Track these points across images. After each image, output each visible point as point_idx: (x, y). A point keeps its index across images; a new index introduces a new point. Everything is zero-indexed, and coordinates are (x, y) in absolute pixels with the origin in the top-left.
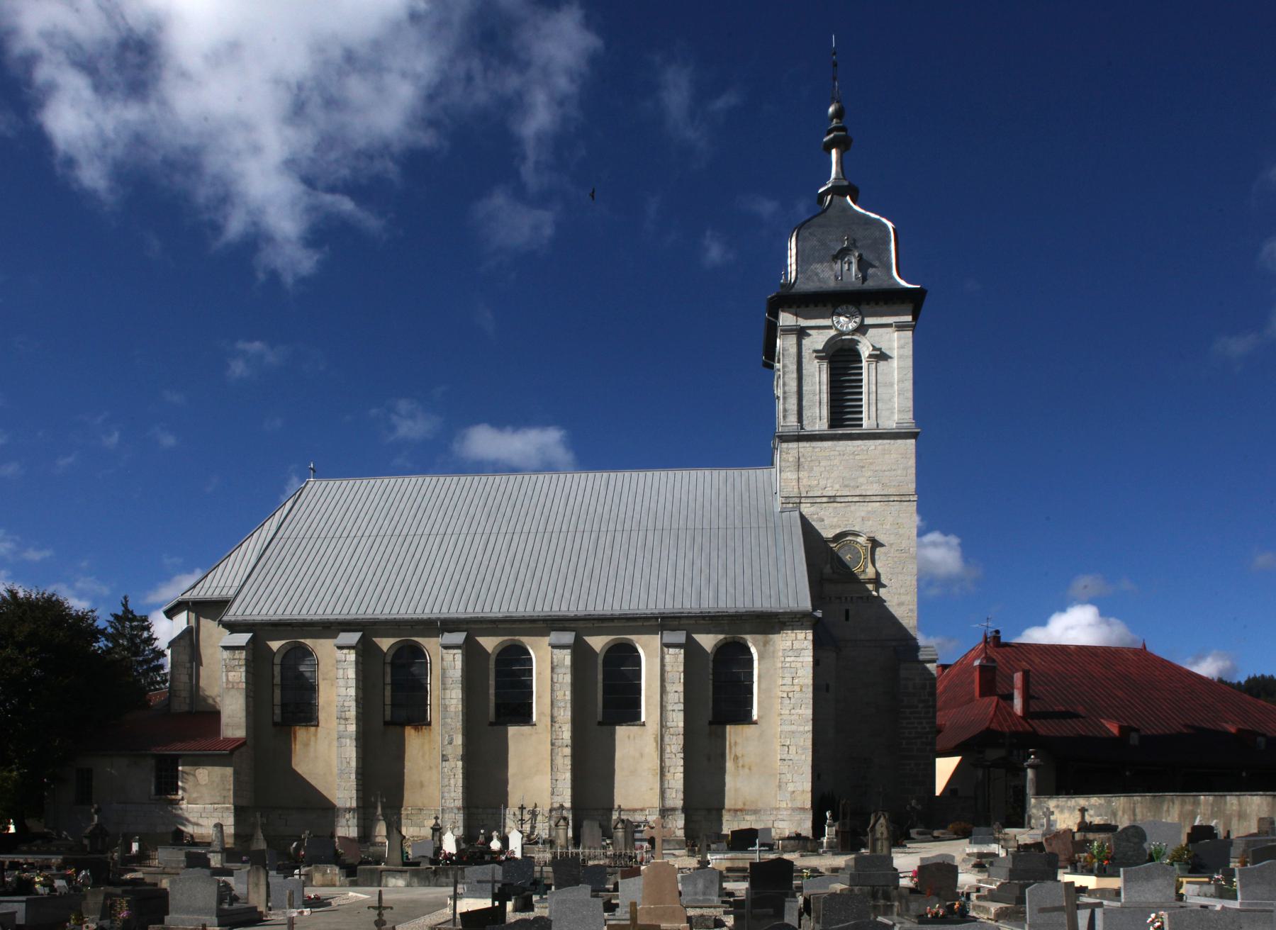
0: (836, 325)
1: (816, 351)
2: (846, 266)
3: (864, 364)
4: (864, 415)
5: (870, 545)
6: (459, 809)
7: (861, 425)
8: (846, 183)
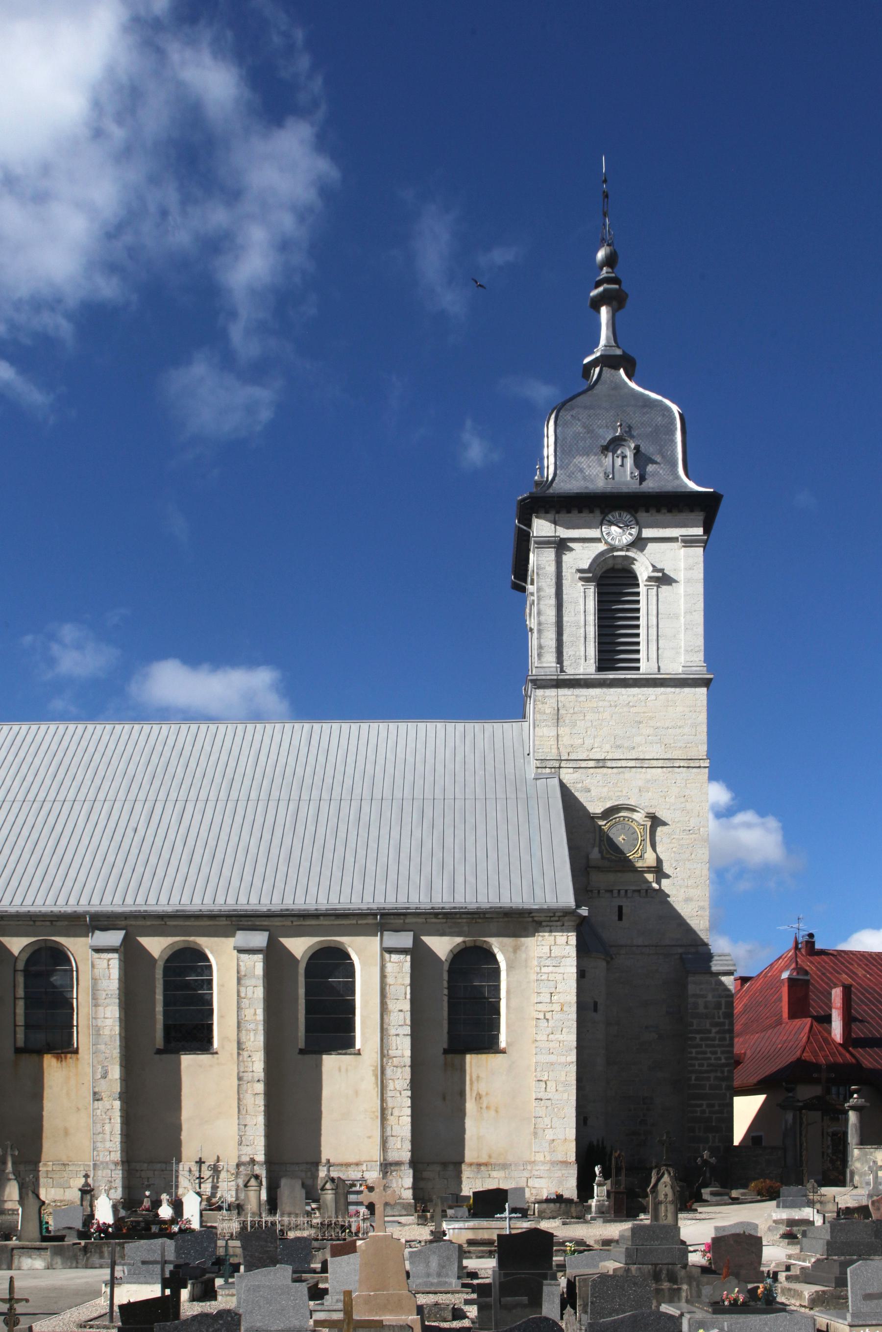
0: (606, 537)
1: (580, 571)
2: (619, 461)
3: (642, 589)
4: (642, 656)
5: (649, 824)
6: (116, 1164)
7: (638, 669)
8: (619, 352)
